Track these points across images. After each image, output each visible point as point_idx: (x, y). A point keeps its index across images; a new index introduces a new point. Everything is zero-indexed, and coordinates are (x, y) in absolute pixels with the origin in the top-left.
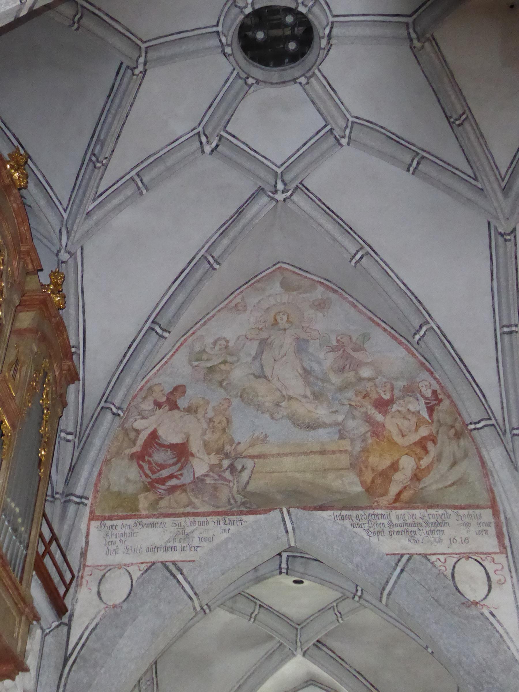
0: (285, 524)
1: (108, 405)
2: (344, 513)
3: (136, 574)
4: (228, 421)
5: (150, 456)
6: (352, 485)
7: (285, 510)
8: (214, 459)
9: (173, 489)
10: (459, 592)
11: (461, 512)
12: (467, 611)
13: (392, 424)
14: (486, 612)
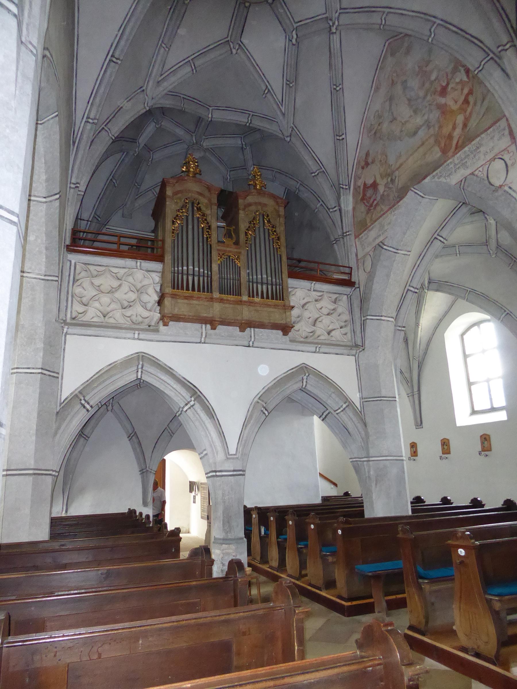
0: (418, 194)
1: (365, 318)
2: (434, 173)
3: (371, 253)
4: (386, 156)
5: (203, 552)
6: (437, 153)
7: (412, 189)
8: (385, 181)
9: (377, 205)
10: (492, 185)
11: (489, 132)
12: (496, 194)
13: (448, 101)
14: (506, 188)
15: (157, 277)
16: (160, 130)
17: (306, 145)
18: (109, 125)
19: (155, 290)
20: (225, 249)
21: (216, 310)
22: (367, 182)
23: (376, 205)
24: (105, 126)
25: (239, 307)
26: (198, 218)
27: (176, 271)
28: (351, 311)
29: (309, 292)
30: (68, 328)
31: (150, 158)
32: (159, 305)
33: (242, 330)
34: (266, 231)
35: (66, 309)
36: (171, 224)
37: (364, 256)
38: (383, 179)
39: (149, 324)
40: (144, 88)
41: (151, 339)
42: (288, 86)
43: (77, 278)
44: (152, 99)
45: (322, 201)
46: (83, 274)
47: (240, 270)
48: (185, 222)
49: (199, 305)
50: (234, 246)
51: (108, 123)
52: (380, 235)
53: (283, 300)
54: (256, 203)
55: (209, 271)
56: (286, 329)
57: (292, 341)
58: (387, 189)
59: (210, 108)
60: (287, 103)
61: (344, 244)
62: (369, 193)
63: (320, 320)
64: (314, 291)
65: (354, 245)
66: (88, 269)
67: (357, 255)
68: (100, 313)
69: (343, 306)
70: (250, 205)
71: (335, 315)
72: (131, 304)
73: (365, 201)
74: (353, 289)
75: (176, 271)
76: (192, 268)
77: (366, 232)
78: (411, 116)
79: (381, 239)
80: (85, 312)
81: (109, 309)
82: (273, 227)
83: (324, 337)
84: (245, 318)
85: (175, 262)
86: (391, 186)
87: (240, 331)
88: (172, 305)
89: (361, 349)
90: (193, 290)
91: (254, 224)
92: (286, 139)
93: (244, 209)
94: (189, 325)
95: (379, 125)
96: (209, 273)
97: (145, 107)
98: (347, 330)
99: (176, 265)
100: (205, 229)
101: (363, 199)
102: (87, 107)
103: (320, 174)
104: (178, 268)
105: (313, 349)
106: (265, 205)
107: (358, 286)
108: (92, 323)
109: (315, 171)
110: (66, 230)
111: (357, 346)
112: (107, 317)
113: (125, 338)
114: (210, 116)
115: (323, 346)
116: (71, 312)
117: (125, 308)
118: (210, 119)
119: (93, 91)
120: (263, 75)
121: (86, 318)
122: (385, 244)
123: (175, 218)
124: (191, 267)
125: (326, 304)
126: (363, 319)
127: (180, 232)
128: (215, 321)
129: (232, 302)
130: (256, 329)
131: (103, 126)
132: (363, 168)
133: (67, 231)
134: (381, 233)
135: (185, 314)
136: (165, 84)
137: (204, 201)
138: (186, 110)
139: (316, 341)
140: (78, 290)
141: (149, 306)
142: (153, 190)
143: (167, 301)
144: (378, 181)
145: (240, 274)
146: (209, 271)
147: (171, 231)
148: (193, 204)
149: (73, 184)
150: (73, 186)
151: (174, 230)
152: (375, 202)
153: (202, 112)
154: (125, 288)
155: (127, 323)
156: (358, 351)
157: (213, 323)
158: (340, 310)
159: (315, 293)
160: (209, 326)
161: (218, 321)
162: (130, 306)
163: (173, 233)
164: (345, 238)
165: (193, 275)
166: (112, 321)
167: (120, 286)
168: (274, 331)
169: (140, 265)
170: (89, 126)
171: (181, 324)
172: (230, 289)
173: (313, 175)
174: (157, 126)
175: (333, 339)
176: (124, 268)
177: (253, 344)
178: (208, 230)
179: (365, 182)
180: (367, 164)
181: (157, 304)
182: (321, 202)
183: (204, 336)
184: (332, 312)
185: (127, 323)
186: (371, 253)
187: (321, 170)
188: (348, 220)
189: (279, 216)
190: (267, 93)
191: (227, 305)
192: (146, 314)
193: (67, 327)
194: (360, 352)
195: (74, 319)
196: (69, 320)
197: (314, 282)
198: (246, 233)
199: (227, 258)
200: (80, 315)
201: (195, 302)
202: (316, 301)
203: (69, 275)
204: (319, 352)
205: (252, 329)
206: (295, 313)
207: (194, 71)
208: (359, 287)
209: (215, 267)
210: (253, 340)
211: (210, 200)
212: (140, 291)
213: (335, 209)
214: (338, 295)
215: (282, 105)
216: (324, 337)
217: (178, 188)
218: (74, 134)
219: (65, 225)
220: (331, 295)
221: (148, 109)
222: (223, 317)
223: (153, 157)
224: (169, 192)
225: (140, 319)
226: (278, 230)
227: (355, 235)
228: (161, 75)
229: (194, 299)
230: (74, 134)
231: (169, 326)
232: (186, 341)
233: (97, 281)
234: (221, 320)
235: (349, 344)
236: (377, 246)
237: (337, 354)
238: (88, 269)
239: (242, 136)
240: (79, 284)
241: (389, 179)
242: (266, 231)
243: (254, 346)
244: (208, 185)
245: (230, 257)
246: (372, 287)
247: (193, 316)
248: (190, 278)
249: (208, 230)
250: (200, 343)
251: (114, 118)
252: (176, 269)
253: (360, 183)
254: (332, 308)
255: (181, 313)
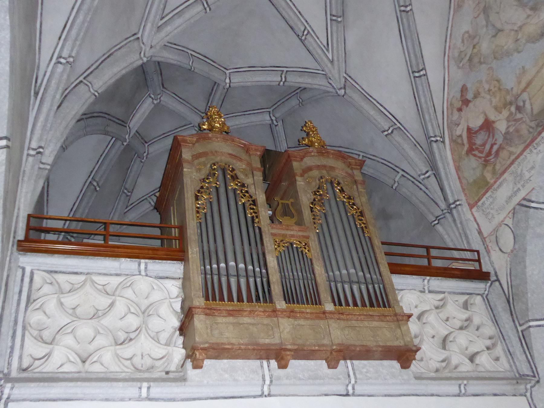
3: (509, 222)
4: (498, 81)
8: (505, 113)
15: (174, 288)
16: (158, 109)
17: (367, 97)
18: (90, 78)
19: (174, 310)
20: (283, 232)
21: (285, 330)
22: (471, 126)
23: (497, 152)
24: (85, 78)
25: (322, 323)
26: (235, 190)
27: (209, 272)
28: (496, 321)
29: (422, 294)
30: (12, 388)
31: (145, 152)
32: (181, 334)
33: (332, 364)
34: (341, 204)
35: (12, 352)
36: (194, 199)
37: (496, 230)
38: (501, 113)
39: (167, 370)
40: (139, 35)
41: (172, 396)
42: (334, 22)
43: (33, 297)
44: (151, 47)
45: (403, 170)
46: (47, 289)
47: (312, 264)
48: (214, 196)
49: (252, 325)
50: (296, 228)
51: (88, 75)
52: (519, 189)
53: (390, 307)
54: (318, 167)
55: (263, 268)
56: (405, 355)
57: (419, 378)
58: (513, 123)
59: (227, 72)
60: (335, 45)
61: (454, 221)
62: (479, 140)
63: (451, 338)
64: (430, 292)
65: (472, 219)
66: (54, 281)
67: (480, 232)
68: (76, 356)
69: (480, 314)
70: (310, 169)
71: (472, 328)
72: (133, 336)
73: (476, 152)
74: (489, 284)
75: (209, 272)
76: (235, 267)
77: (489, 194)
78: (529, 16)
79: (522, 194)
80: (48, 356)
81: (92, 348)
82: (349, 198)
83: (466, 367)
84: (336, 341)
85: (206, 256)
86: (519, 116)
87: (329, 367)
88: (207, 328)
89: (533, 382)
90: (240, 299)
91: (320, 195)
92: (339, 92)
93: (302, 175)
94: (239, 363)
95: (474, 47)
96: (264, 271)
97: (141, 58)
98: (499, 350)
99: (207, 261)
100: (247, 205)
101: (470, 151)
102: (58, 44)
103: (395, 132)
104: (211, 265)
105: (455, 390)
106: (332, 168)
107: (495, 278)
108: (61, 376)
109: (387, 128)
110: (17, 217)
111: (521, 378)
112: (87, 363)
113: (122, 400)
114: (228, 81)
115: (471, 382)
116: (21, 357)
117: (121, 344)
118: (228, 85)
119: (67, 22)
120: (299, 12)
121: (50, 367)
122: (533, 199)
123: (199, 191)
124: (232, 263)
125: (455, 311)
126: (520, 329)
127: (223, 185)
128: (286, 350)
129: (309, 316)
130: (354, 361)
131: (81, 78)
132: (460, 110)
133: (21, 219)
134: (519, 186)
135: (233, 341)
136: (169, 28)
137: (240, 166)
138: (196, 71)
139: (454, 375)
140: (35, 318)
141: (164, 337)
142: (149, 199)
143: (199, 322)
144: (492, 117)
145: (313, 271)
146: (263, 268)
147: (195, 209)
148: (224, 171)
149: (33, 149)
150: (32, 152)
151: (198, 208)
152: (495, 148)
153: (216, 76)
154: (120, 307)
155: (126, 369)
156: (529, 386)
157: (280, 355)
158: (477, 320)
159: (431, 296)
160: (274, 363)
161: (290, 350)
162: (131, 340)
163: (198, 212)
164: (454, 211)
165: (238, 276)
166: (97, 368)
167: (112, 305)
168: (386, 363)
169: (146, 268)
170: (60, 68)
171: (225, 363)
172: (303, 295)
173: (386, 133)
174: (155, 102)
175: (481, 369)
176: (117, 275)
177: (353, 389)
178: (252, 206)
179: (468, 126)
180: (466, 102)
181: (178, 332)
182: (401, 173)
183: (268, 382)
184: (466, 324)
185: (127, 370)
186: (509, 222)
187: (396, 127)
188: (453, 187)
189: (356, 182)
190: (307, 35)
191: (302, 322)
192: (159, 352)
193: (9, 385)
194: (532, 387)
195: (25, 370)
196: (14, 374)
197: (428, 278)
198: (311, 208)
199: (288, 247)
200: (37, 362)
201: (246, 320)
202: (437, 308)
203: (20, 292)
204: (465, 395)
205: (349, 362)
206: (413, 326)
207: (208, 9)
208: (498, 280)
209: (272, 262)
210: (353, 381)
211: (249, 164)
212: (146, 313)
213: (427, 175)
214: (467, 296)
215: (328, 50)
216: (466, 367)
217: (199, 148)
218: (36, 82)
219: (16, 210)
220: (457, 297)
221: (145, 60)
222: (299, 342)
223: (148, 151)
224: (186, 154)
225: (148, 362)
226: (357, 201)
227: (469, 204)
228: (162, 18)
229: (245, 313)
230: (36, 82)
231: (205, 368)
232: (236, 394)
233: (69, 301)
234: (296, 347)
235: (509, 375)
236: (518, 207)
237: (495, 395)
238: (54, 281)
239: (271, 110)
240: (37, 307)
241: (513, 109)
242: (341, 204)
243: (357, 392)
244: (244, 144)
245: (292, 244)
246: (524, 273)
247: (247, 345)
248: (233, 281)
249: (252, 206)
250: (261, 396)
251: (97, 70)
252: (208, 267)
253: (461, 130)
254: (464, 316)
255: (225, 341)
